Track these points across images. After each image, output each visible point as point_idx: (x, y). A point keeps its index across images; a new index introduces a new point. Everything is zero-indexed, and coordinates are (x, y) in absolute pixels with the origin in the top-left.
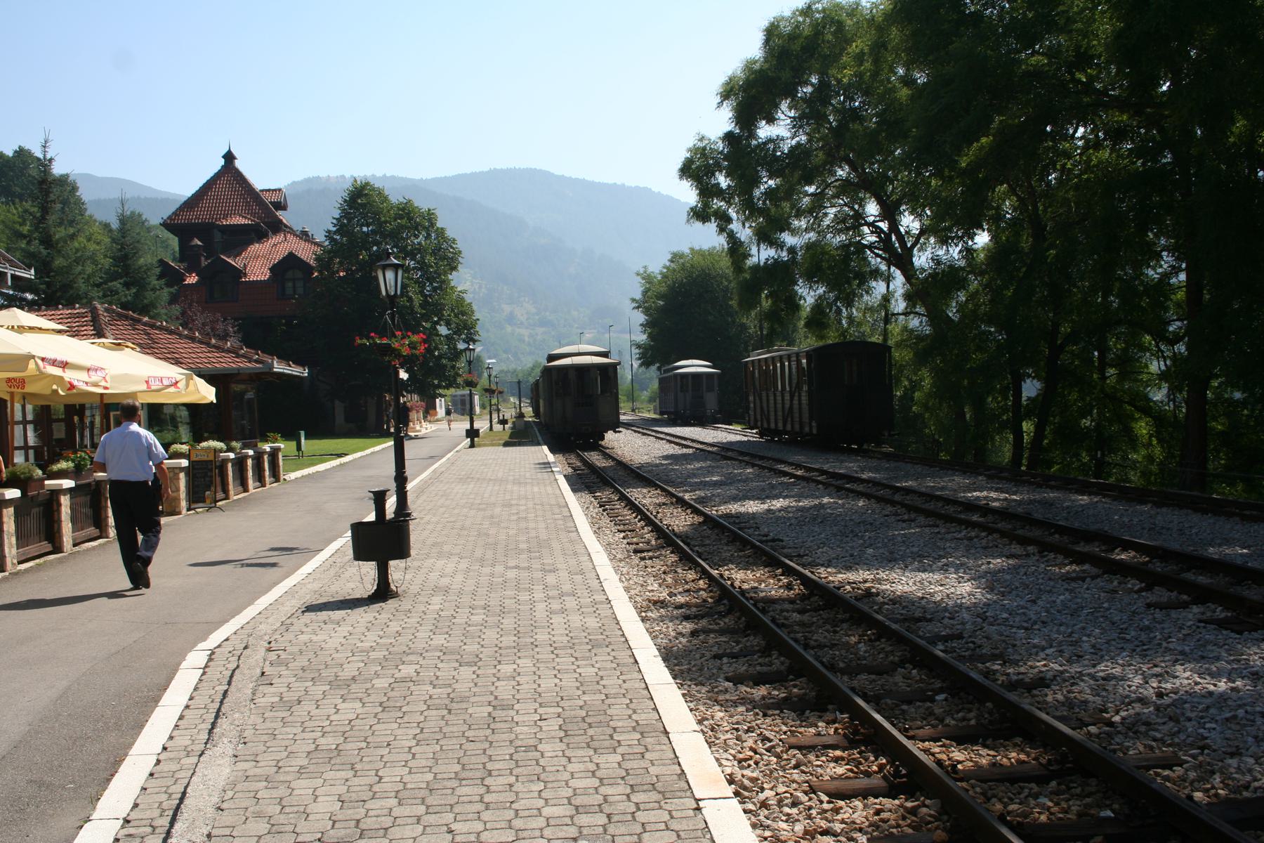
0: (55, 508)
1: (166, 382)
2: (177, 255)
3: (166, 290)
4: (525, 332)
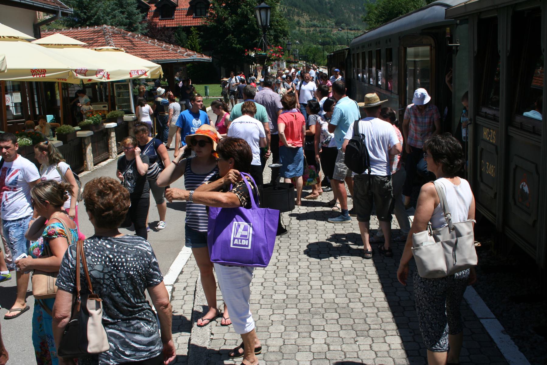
0: (83, 147)
1: (140, 73)
3: (141, 15)
4: (304, 30)
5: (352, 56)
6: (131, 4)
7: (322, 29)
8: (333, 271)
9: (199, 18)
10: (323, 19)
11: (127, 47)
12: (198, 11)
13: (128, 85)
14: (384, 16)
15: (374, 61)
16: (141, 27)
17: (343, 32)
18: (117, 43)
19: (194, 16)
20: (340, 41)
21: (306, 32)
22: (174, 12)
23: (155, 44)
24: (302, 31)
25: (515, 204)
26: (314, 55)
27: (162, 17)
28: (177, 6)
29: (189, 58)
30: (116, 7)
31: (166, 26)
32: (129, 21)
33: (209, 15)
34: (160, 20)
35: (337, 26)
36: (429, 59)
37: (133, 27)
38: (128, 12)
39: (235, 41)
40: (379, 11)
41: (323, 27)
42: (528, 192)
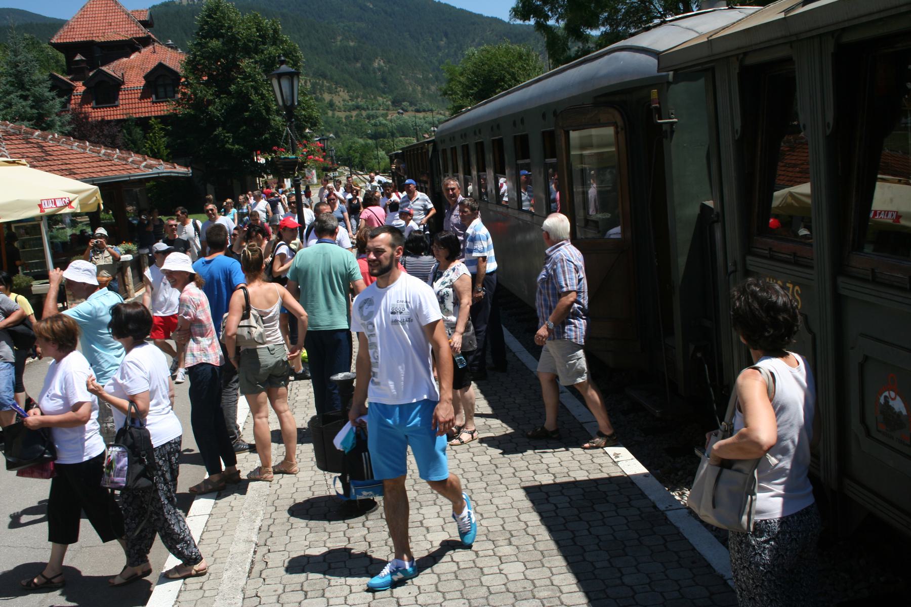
1: (59, 204)
2: (65, 68)
3: (58, 100)
5: (440, 153)
6: (40, 83)
7: (371, 112)
8: (491, 593)
9: (162, 102)
10: (372, 96)
11: (34, 158)
12: (161, 90)
13: (39, 225)
14: (475, 86)
15: (473, 160)
16: (60, 121)
17: (406, 116)
18: (13, 151)
19: (154, 100)
20: (403, 131)
21: (345, 118)
22: (119, 94)
23: (85, 149)
24: (339, 118)
25: (868, 433)
26: (362, 156)
27: (97, 104)
28: (123, 83)
29: (150, 171)
30: (12, 88)
31: (106, 118)
32: (36, 111)
33: (180, 96)
34: (93, 108)
35: (396, 106)
36: (613, 149)
37: (45, 123)
38: (34, 96)
39: (229, 139)
40: (468, 78)
41: (372, 110)
42: (904, 412)
